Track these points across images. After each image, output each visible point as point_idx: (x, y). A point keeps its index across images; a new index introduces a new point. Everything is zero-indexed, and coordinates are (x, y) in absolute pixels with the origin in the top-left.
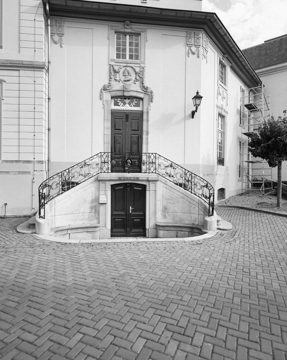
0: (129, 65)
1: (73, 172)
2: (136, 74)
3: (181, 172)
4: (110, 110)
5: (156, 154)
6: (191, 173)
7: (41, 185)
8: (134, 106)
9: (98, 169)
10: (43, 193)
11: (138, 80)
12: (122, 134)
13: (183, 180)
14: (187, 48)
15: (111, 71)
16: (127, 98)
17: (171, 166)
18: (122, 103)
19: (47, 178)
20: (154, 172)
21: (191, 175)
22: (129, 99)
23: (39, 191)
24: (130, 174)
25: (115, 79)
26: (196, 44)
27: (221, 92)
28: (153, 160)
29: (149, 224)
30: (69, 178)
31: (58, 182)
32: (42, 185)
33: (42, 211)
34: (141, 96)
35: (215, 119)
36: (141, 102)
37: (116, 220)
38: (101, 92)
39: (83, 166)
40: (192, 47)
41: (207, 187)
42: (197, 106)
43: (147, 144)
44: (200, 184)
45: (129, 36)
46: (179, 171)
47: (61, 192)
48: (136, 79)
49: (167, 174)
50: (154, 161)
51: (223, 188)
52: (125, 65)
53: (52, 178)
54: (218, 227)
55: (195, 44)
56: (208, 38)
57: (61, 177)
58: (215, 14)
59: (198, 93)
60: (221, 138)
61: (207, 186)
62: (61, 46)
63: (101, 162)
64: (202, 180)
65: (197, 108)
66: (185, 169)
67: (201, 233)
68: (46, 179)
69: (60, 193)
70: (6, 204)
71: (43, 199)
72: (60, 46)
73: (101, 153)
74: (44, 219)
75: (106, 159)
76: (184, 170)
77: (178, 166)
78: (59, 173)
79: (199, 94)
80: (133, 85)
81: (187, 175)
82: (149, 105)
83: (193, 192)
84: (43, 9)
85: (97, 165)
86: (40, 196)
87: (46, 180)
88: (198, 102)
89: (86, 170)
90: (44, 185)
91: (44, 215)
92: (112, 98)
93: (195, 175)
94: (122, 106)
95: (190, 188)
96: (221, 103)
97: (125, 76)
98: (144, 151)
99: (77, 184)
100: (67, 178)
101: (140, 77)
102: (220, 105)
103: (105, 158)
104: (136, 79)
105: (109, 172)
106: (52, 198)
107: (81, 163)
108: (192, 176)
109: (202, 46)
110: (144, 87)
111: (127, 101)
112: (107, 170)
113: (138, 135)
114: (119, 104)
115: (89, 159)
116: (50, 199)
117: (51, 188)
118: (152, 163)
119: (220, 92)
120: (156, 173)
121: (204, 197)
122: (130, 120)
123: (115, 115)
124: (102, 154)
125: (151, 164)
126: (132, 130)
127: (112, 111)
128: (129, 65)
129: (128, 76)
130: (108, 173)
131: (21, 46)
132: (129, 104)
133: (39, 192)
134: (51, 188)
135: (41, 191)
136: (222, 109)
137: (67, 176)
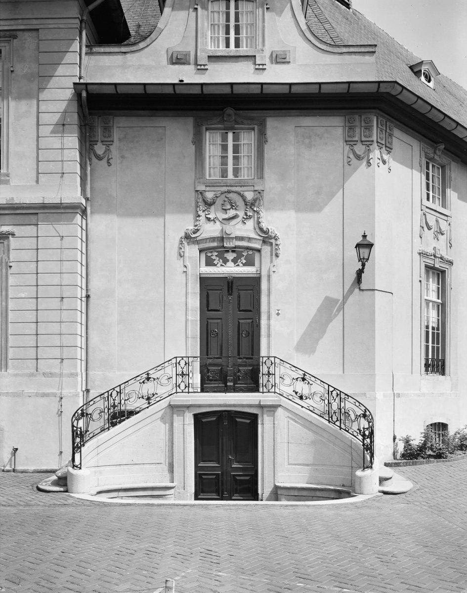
0: (234, 189)
1: (126, 392)
2: (246, 205)
3: (282, 387)
4: (197, 275)
5: (276, 359)
6: (339, 392)
7: (74, 415)
8: (244, 265)
9: (170, 387)
10: (79, 427)
11: (250, 217)
12: (221, 319)
13: (325, 405)
14: (347, 148)
15: (199, 204)
16: (230, 251)
17: (304, 379)
18: (221, 261)
19: (85, 403)
20: (273, 390)
21: (339, 396)
22: (233, 251)
23: (72, 423)
24: (228, 394)
25: (207, 218)
26: (363, 139)
27: (432, 223)
28: (271, 369)
29: (265, 487)
30: (120, 401)
31: (103, 408)
32: (76, 415)
33: (77, 456)
34: (257, 246)
35: (416, 278)
36: (257, 255)
37: (204, 477)
38: (181, 243)
39: (298, 379)
40: (356, 144)
41: (364, 418)
42: (363, 261)
43: (269, 336)
44: (354, 412)
45: (234, 133)
46: (318, 388)
47: (107, 426)
48: (247, 215)
49: (296, 393)
51: (443, 424)
52: (225, 189)
53: (91, 403)
54: (382, 488)
55: (363, 140)
56: (390, 121)
57: (107, 399)
58: (396, 82)
59: (364, 236)
60: (438, 317)
61: (364, 416)
62: (109, 164)
63: (177, 375)
64: (357, 404)
65: (363, 265)
66: (329, 385)
67: (348, 494)
68: (82, 405)
69: (106, 428)
70: (17, 449)
71: (79, 438)
72: (106, 164)
73: (176, 358)
74: (80, 468)
75: (185, 367)
76: (326, 386)
77: (317, 380)
78: (103, 394)
79: (368, 238)
80: (240, 226)
81: (186, 385)
82: (272, 262)
83: (343, 426)
84: (77, 102)
85: (169, 379)
86: (73, 431)
87: (83, 406)
88: (364, 252)
89: (149, 388)
90: (83, 414)
91: (81, 464)
92: (201, 251)
93: (346, 395)
94: (221, 265)
95: (337, 420)
96: (430, 244)
97: (226, 210)
98: (263, 353)
99: (131, 413)
100: (117, 402)
101: (254, 211)
102: (430, 250)
103: (183, 367)
104: (246, 214)
105: (190, 391)
106: (93, 436)
107: (141, 376)
108: (340, 398)
109: (377, 142)
110: (261, 229)
111: (230, 256)
112: (187, 388)
113: (251, 321)
114: (215, 262)
115: (156, 369)
116: (89, 438)
117: (91, 419)
119: (427, 223)
120: (275, 392)
121: (360, 434)
122: (235, 293)
123: (206, 284)
124: (178, 359)
125: (181, 377)
127: (202, 276)
128: (234, 189)
129: (231, 210)
130: (189, 392)
131: (40, 171)
132: (235, 261)
133: (73, 426)
134: (91, 419)
135: (75, 424)
136: (435, 256)
137: (117, 398)
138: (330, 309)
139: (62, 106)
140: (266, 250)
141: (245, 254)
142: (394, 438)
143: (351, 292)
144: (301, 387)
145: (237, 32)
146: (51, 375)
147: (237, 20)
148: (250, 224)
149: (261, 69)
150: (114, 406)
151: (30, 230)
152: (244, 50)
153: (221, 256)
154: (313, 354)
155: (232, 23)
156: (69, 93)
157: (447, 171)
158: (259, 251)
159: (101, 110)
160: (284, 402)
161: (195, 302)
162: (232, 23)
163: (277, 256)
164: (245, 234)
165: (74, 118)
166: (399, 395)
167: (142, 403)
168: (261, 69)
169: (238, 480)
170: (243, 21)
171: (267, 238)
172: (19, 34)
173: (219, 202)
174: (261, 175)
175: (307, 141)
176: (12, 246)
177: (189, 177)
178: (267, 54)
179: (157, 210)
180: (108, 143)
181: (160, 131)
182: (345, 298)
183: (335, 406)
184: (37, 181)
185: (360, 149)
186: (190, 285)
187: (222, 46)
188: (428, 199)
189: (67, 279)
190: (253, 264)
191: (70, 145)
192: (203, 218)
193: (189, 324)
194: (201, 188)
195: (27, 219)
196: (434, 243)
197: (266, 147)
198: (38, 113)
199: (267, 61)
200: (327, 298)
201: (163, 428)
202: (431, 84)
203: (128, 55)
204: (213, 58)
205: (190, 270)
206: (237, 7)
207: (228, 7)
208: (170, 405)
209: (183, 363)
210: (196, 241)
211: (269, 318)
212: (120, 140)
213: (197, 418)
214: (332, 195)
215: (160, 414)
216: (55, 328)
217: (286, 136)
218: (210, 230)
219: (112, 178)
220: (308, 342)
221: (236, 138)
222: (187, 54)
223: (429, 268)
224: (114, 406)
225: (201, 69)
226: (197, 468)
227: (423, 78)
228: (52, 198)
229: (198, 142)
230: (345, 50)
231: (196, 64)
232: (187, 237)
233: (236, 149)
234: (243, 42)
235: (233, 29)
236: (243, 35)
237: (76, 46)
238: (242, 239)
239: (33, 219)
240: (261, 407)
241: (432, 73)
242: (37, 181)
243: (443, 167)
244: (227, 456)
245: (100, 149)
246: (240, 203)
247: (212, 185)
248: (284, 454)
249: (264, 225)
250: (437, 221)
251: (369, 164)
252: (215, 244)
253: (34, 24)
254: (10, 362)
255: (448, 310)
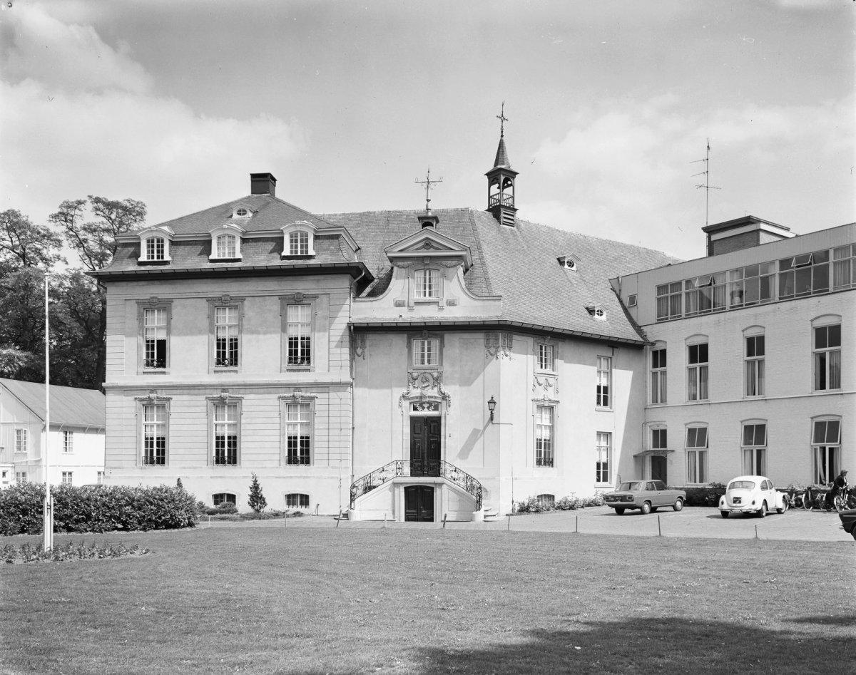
0: (427, 371)
42: (492, 410)
43: (445, 447)
46: (462, 475)
50: (400, 467)
52: (423, 371)
80: (430, 390)
88: (492, 405)
89: (383, 475)
99: (375, 487)
118: (399, 468)
123: (414, 421)
126: (764, 328)
128: (427, 371)
132: (428, 408)
138: (476, 435)
139: (341, 332)
140: (444, 403)
141: (433, 404)
142: (513, 502)
143: (487, 425)
144: (454, 475)
145: (430, 288)
146: (336, 468)
147: (430, 282)
148: (436, 389)
149: (441, 309)
150: (368, 483)
151: (326, 395)
152: (433, 298)
153: (421, 405)
154: (249, 503)
155: (427, 283)
156: (345, 326)
157: (556, 349)
158: (440, 403)
159: (359, 333)
160: (446, 481)
161: (408, 430)
162: (427, 283)
163: (449, 406)
164: (433, 395)
165: (347, 338)
166: (516, 479)
167: (381, 482)
168: (441, 309)
169: (415, 509)
170: (433, 283)
171: (445, 397)
172: (320, 296)
173: (420, 378)
174: (441, 364)
175: (465, 346)
176: (316, 402)
177: (404, 366)
178: (445, 300)
179: (388, 385)
180: (363, 347)
181: (390, 341)
182: (485, 428)
183: (469, 483)
184: (329, 371)
185: (492, 350)
186: (405, 422)
187: (422, 296)
188: (542, 367)
189: (343, 420)
190: (438, 410)
191: (345, 352)
192: (411, 387)
193: (404, 441)
194: (411, 371)
195: (324, 390)
196: (545, 393)
197: (444, 350)
198: (329, 336)
199: (445, 304)
200: (475, 429)
201: (390, 493)
202: (574, 268)
203: (374, 302)
204: (417, 303)
205: (405, 415)
206: (430, 275)
207: (425, 275)
208: (164, 309)
209: (399, 463)
210: (409, 399)
211: (445, 438)
212: (370, 346)
213: (406, 489)
214: (478, 375)
215: (388, 488)
216: (337, 444)
217: (454, 343)
218: (415, 392)
219: (365, 366)
220: (464, 453)
221: (429, 344)
222: (404, 301)
223: (540, 407)
224: (368, 483)
225: (411, 309)
226: (406, 513)
227: (566, 266)
228: (336, 380)
229: (409, 346)
230: (485, 298)
231: (408, 306)
232: (403, 396)
233: (429, 350)
234: (433, 294)
235: (428, 287)
236: (433, 290)
237: (348, 302)
238: (432, 397)
239: (327, 389)
240: (435, 484)
241: (574, 260)
242: (329, 371)
243: (553, 346)
244: (420, 503)
245: (359, 351)
246: (431, 378)
247: (417, 369)
248: (445, 503)
249: (443, 391)
250: (546, 379)
251: (497, 358)
252: (418, 400)
253: (327, 291)
254: (315, 461)
255: (555, 429)
